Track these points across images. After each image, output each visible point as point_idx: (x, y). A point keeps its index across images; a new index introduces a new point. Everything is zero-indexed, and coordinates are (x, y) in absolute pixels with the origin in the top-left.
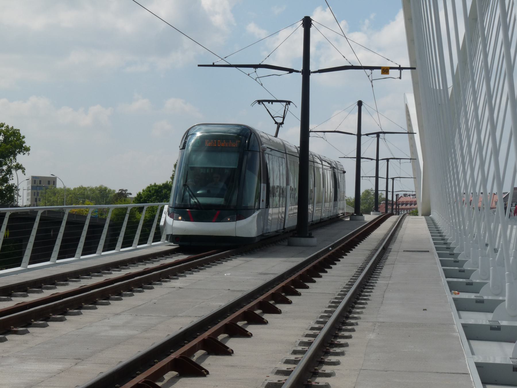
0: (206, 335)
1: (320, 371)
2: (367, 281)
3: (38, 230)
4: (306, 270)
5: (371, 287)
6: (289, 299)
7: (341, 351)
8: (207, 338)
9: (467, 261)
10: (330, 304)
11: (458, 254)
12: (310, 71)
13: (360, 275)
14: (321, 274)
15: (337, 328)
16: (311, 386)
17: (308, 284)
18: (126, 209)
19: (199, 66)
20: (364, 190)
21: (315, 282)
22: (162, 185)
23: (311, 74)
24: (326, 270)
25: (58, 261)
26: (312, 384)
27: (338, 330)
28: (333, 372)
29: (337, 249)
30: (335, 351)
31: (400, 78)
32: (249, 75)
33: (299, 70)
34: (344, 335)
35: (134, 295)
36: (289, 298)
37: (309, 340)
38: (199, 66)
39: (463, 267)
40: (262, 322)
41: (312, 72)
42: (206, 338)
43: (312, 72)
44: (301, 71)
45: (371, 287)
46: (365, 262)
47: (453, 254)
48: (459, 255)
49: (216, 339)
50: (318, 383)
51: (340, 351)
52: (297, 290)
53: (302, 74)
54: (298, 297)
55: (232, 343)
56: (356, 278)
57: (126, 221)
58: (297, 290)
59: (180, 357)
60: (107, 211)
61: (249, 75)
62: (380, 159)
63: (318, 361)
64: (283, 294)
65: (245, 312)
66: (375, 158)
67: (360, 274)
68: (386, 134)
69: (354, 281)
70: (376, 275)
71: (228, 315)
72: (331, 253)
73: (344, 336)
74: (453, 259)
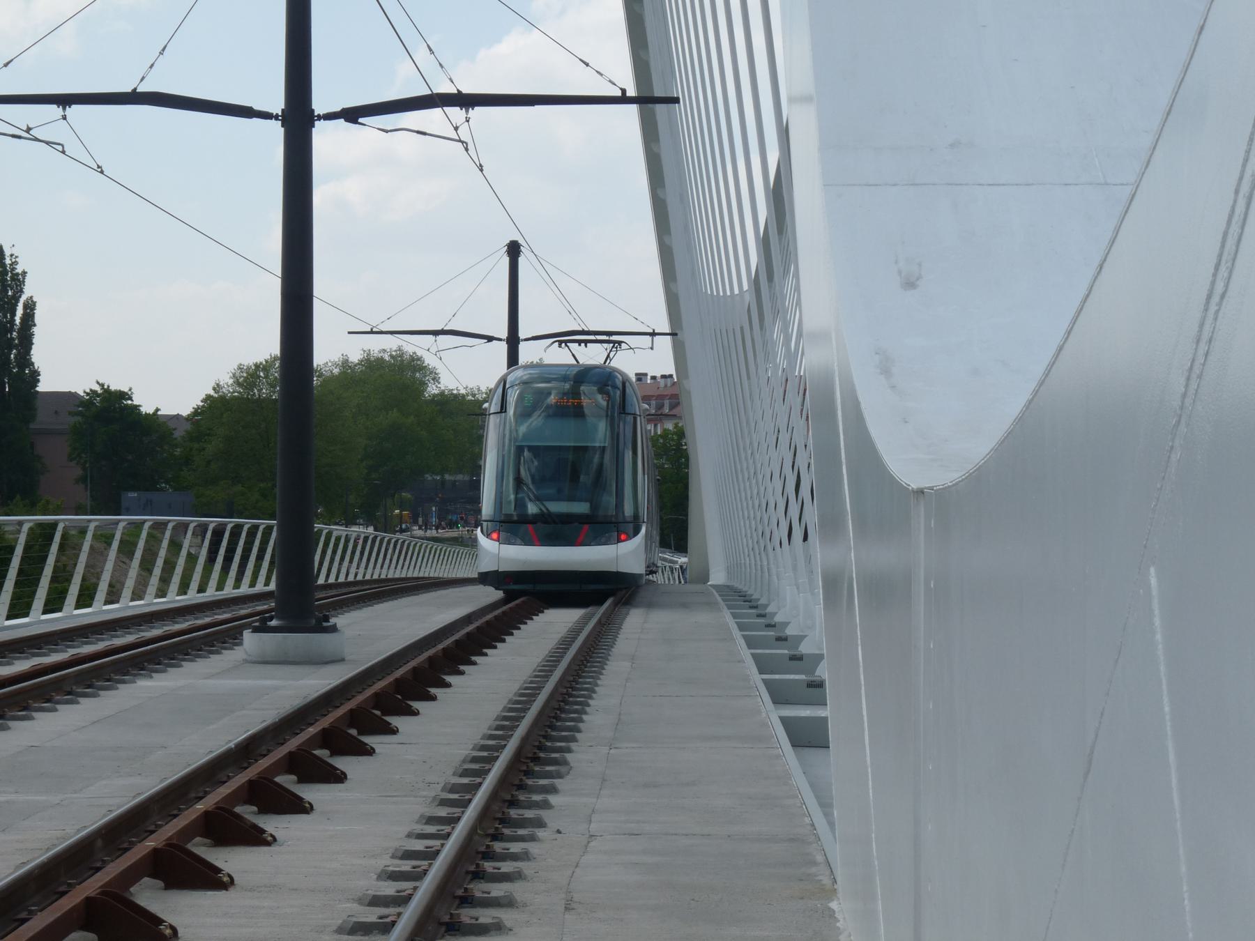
0: (92, 886)
1: (478, 894)
2: (551, 722)
3: (227, 547)
4: (409, 668)
5: (563, 744)
6: (391, 724)
7: (506, 894)
8: (164, 846)
9: (805, 636)
10: (483, 742)
11: (801, 638)
12: (313, 111)
13: (556, 667)
14: (433, 691)
15: (456, 894)
16: (484, 874)
17: (416, 705)
18: (54, 525)
19: (349, 333)
20: (25, 292)
21: (448, 685)
22: (283, 129)
23: (317, 123)
24: (474, 658)
25: (132, 604)
26: (460, 922)
27: (519, 789)
28: (509, 894)
29: (487, 619)
30: (499, 869)
31: (652, 348)
32: (428, 350)
33: (270, 111)
34: (511, 851)
35: (35, 717)
36: (370, 740)
37: (427, 848)
38: (349, 333)
39: (799, 650)
40: (257, 838)
41: (320, 117)
42: (162, 845)
43: (320, 117)
44: (280, 114)
45: (563, 744)
46: (568, 638)
47: (774, 626)
48: (802, 641)
49: (127, 895)
50: (489, 893)
51: (503, 894)
52: (261, 825)
53: (282, 126)
54: (303, 817)
55: (229, 860)
56: (555, 663)
57: (53, 553)
58: (388, 719)
59: (103, 893)
60: (225, 525)
61: (428, 350)
62: (522, 335)
63: (468, 872)
64: (378, 713)
65: (291, 754)
66: (504, 333)
67: (556, 666)
68: (478, 112)
69: (531, 701)
70: (589, 677)
71: (180, 808)
72: (482, 624)
73: (492, 897)
74: (786, 652)
